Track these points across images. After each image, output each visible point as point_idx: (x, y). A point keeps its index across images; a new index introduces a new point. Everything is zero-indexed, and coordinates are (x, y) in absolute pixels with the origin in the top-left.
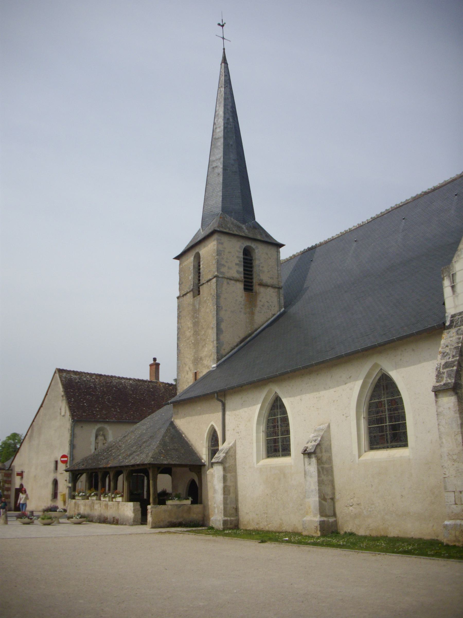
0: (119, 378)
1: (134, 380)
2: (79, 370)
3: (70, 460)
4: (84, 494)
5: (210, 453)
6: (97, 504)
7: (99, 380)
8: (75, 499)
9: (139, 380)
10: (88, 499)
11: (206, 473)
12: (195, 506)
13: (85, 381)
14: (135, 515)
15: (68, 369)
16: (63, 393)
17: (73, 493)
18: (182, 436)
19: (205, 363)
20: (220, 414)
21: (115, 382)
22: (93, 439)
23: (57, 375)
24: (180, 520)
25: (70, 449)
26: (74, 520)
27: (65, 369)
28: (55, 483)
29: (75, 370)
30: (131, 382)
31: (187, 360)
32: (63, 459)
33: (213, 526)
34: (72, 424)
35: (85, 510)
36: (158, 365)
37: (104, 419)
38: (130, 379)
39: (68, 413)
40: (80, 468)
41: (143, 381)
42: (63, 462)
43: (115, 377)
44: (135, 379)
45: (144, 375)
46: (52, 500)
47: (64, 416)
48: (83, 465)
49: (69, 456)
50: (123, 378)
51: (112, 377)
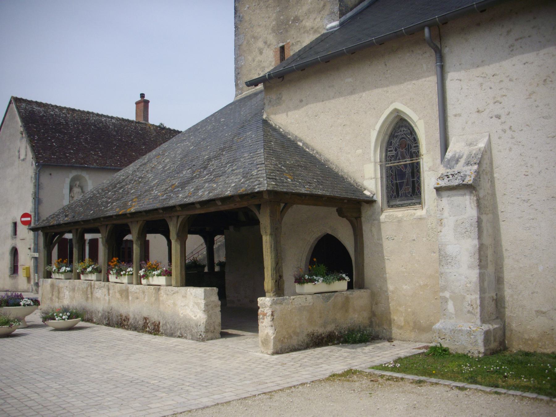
0: (98, 115)
1: (118, 119)
2: (44, 102)
3: (35, 220)
4: (68, 269)
5: (384, 176)
6: (100, 288)
7: (72, 115)
8: (51, 278)
9: (123, 120)
10: (79, 278)
11: (379, 220)
12: (356, 293)
13: (52, 115)
14: (209, 317)
15: (29, 99)
16: (22, 129)
17: (48, 268)
18: (297, 147)
19: (307, 24)
20: (432, 81)
21: (92, 119)
22: (66, 191)
23: (13, 106)
24: (330, 328)
25: (35, 204)
26: (58, 322)
27: (24, 98)
28: (15, 252)
29: (39, 101)
30: (113, 121)
31: (259, 30)
32: (23, 219)
33: (445, 346)
34: (36, 170)
35: (72, 298)
36: (147, 102)
37: (82, 164)
38: (112, 118)
39: (30, 155)
40: (62, 222)
41: (128, 121)
42: (24, 223)
43: (93, 113)
44: (119, 118)
45: (129, 113)
46: (10, 276)
47: (24, 160)
48: (66, 216)
49: (33, 214)
50: (102, 116)
51: (88, 113)
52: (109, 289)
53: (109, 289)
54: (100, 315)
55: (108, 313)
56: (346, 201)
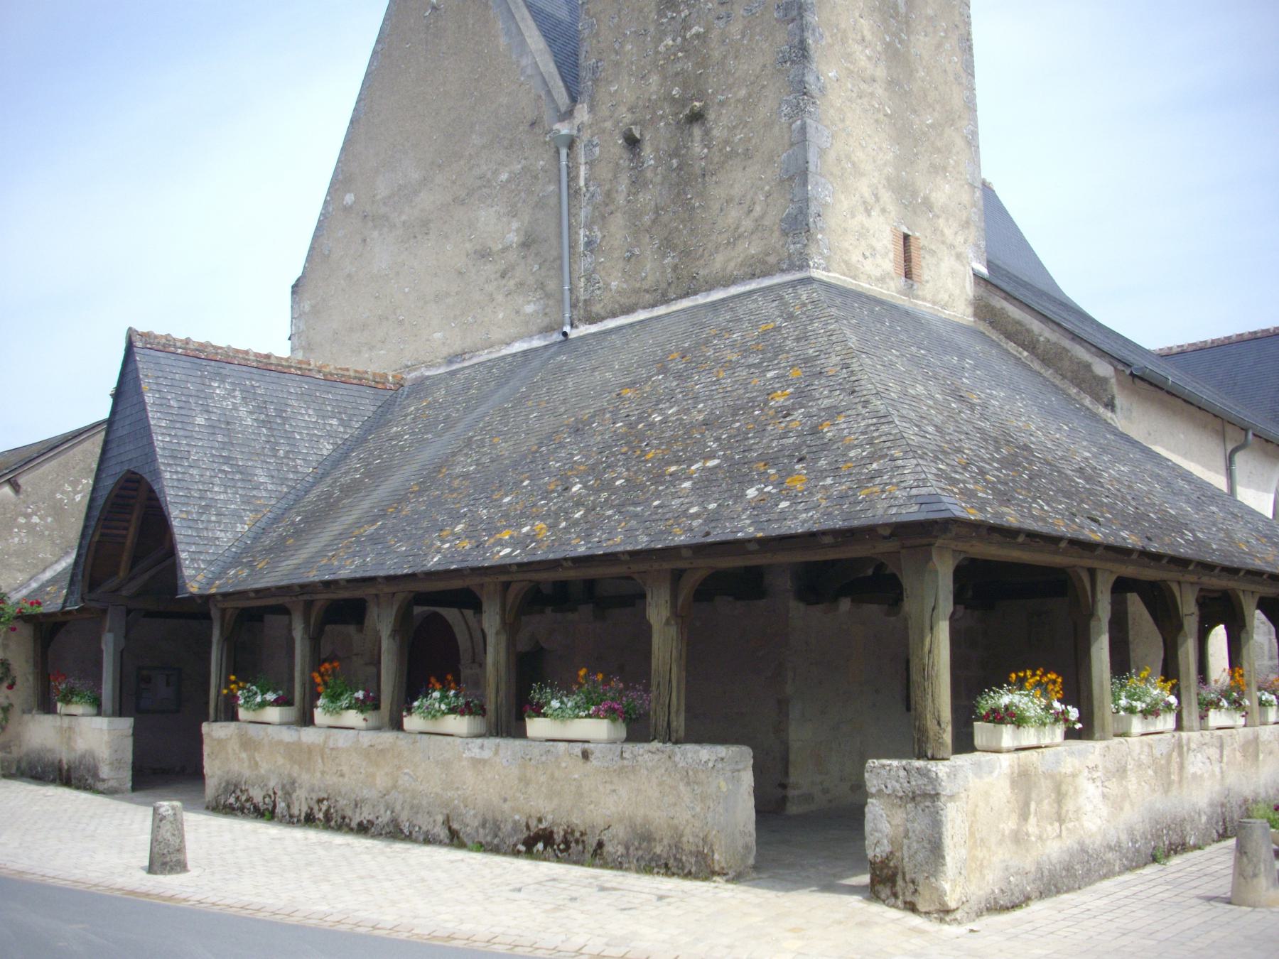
52: (1221, 747)
53: (1221, 747)
54: (1204, 819)
55: (1223, 805)
56: (827, 540)
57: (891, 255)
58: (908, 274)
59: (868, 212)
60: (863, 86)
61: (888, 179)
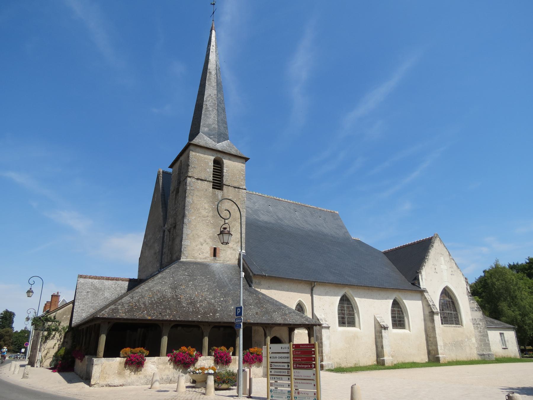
57: (209, 253)
58: (215, 255)
59: (202, 245)
60: (203, 219)
61: (210, 237)
